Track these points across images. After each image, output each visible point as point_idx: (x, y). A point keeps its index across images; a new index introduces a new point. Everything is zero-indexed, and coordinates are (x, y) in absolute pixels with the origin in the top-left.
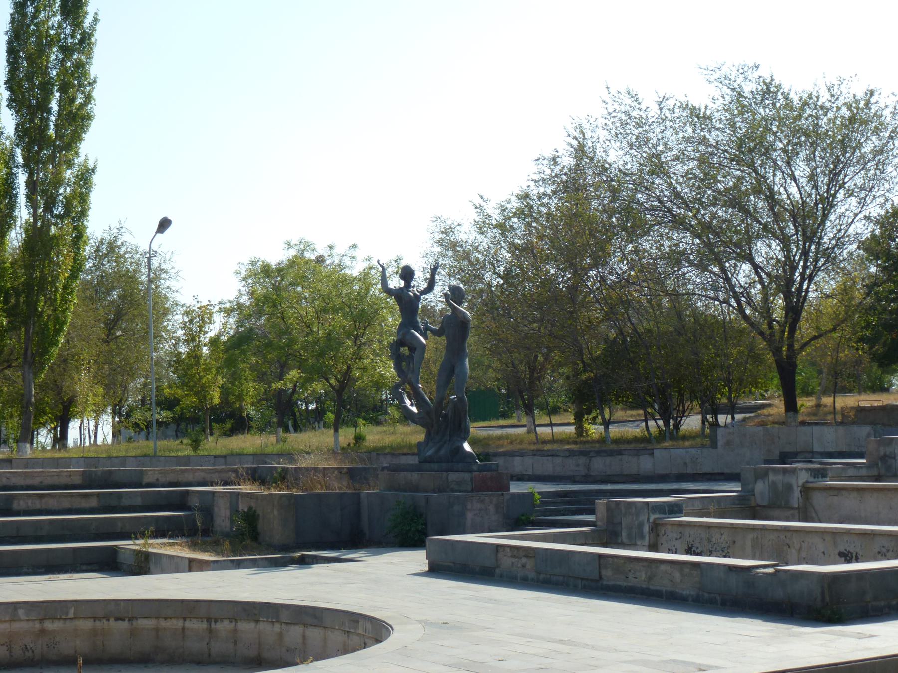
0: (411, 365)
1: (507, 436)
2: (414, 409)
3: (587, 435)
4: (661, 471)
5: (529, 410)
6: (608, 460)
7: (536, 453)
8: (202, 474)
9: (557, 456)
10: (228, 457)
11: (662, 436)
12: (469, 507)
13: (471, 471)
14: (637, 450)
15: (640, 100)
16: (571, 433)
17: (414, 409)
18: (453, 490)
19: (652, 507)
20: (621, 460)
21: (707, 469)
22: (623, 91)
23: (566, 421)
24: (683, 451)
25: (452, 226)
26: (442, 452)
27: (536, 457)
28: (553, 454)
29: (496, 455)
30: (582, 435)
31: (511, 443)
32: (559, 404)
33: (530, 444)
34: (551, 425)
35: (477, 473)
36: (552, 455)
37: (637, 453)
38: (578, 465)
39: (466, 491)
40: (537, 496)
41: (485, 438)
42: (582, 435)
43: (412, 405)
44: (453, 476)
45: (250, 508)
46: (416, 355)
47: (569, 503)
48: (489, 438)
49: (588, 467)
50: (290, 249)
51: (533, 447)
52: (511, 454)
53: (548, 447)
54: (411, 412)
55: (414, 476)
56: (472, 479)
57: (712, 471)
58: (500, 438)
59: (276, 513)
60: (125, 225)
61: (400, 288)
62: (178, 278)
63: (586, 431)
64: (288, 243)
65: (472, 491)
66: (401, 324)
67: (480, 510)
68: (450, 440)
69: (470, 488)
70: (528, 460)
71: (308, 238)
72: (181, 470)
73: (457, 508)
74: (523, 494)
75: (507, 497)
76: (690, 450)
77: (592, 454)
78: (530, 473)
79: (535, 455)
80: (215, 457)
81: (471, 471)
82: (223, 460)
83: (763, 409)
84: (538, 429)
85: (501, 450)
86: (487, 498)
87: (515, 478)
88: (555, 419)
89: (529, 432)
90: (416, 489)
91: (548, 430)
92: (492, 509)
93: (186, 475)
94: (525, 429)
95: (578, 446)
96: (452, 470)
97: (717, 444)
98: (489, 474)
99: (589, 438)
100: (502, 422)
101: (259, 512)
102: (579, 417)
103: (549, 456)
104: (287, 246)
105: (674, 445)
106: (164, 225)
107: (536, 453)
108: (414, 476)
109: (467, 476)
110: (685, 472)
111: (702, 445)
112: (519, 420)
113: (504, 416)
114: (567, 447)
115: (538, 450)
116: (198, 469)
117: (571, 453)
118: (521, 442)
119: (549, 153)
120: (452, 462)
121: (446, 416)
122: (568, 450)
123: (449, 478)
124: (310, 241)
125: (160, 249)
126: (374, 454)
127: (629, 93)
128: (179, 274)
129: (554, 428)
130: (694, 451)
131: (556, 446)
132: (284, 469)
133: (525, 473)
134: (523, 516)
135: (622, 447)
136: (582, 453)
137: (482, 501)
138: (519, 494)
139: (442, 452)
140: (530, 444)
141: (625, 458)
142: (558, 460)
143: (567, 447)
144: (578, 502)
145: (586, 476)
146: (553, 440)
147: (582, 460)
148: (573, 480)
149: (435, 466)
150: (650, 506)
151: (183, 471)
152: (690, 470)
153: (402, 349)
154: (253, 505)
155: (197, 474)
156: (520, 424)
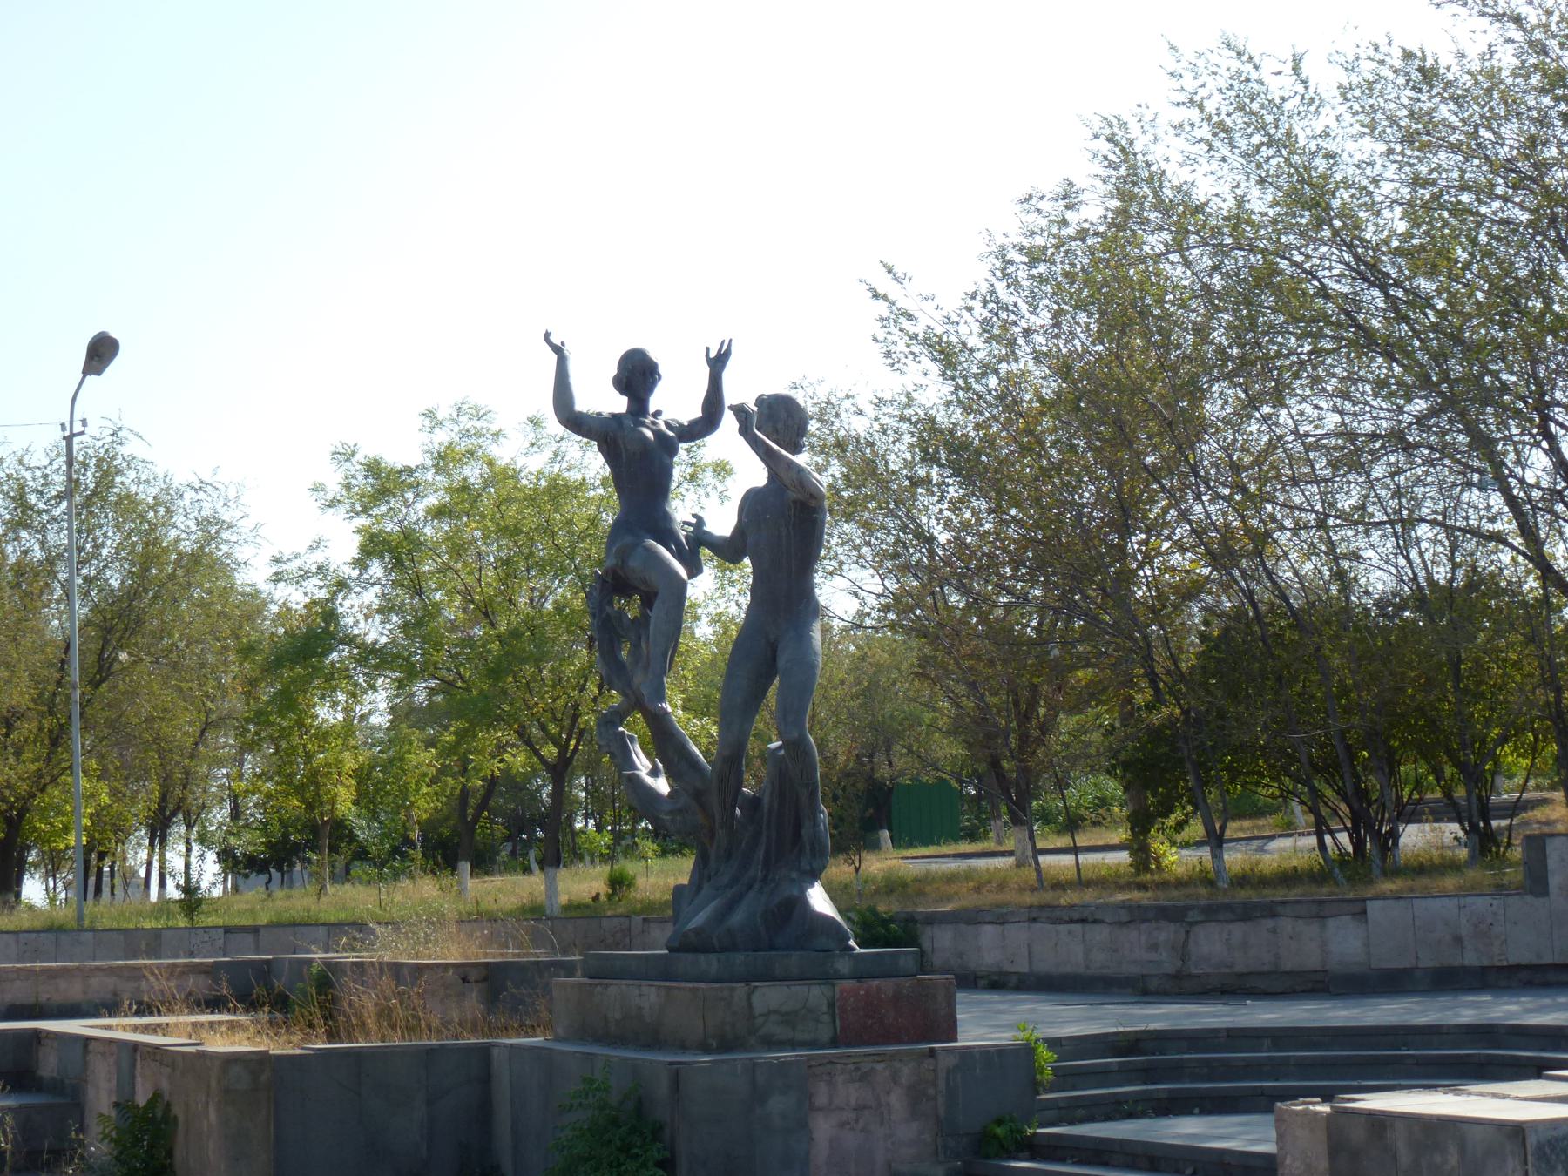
0: (643, 645)
1: (969, 875)
2: (662, 786)
3: (1159, 868)
4: (1388, 958)
5: (1020, 818)
6: (1238, 930)
7: (1039, 914)
8: (111, 982)
9: (1095, 921)
10: (262, 932)
11: (1355, 867)
12: (821, 1099)
13: (828, 978)
14: (1321, 902)
15: (1257, 60)
16: (1119, 864)
17: (662, 786)
18: (771, 1043)
19: (1540, 1147)
20: (1274, 931)
21: (1520, 954)
22: (1215, 42)
23: (1101, 843)
24: (1452, 904)
25: (833, 400)
26: (737, 918)
27: (1038, 926)
28: (1084, 918)
29: (932, 920)
30: (1147, 869)
31: (978, 889)
32: (1082, 811)
33: (1021, 890)
34: (1075, 850)
35: (849, 984)
36: (1083, 921)
37: (1320, 912)
38: (1154, 947)
39: (813, 1044)
40: (1044, 1053)
41: (916, 880)
42: (1147, 869)
43: (654, 773)
44: (769, 996)
45: (156, 1096)
46: (656, 614)
47: (1148, 1073)
48: (925, 880)
49: (1183, 953)
50: (437, 430)
51: (1029, 899)
52: (970, 918)
53: (1068, 898)
54: (652, 793)
55: (648, 996)
56: (831, 1005)
57: (1535, 961)
58: (951, 878)
59: (213, 1116)
60: (126, 423)
61: (615, 417)
62: (258, 540)
63: (1157, 860)
64: (430, 414)
65: (834, 1043)
66: (618, 526)
67: (860, 1108)
68: (765, 878)
69: (825, 1033)
70: (1018, 934)
71: (479, 399)
72: (49, 969)
73: (777, 1104)
74: (1001, 1051)
75: (945, 1062)
76: (1469, 900)
77: (1193, 916)
78: (1022, 967)
79: (1034, 920)
80: (228, 930)
81: (828, 978)
82: (250, 938)
83: (1532, 808)
84: (1041, 859)
85: (947, 908)
86: (880, 1067)
87: (982, 982)
88: (1082, 840)
89: (1019, 865)
90: (653, 1038)
91: (1068, 860)
92: (896, 1100)
93: (63, 984)
94: (1011, 860)
95: (1149, 894)
96: (768, 976)
97: (1547, 884)
98: (888, 985)
99: (1166, 876)
100: (965, 847)
101: (177, 1110)
102: (1141, 823)
103: (1071, 921)
104: (427, 422)
105: (1412, 890)
106: (101, 352)
107: (1039, 914)
108: (648, 996)
109: (816, 994)
110: (1457, 962)
111: (397, 930)
112: (1000, 843)
113: (972, 836)
114: (1120, 897)
115: (1042, 907)
116: (98, 969)
117: (1136, 915)
118: (1001, 887)
119: (1051, 185)
120: (772, 947)
121: (755, 803)
122: (1123, 905)
123: (756, 999)
124: (481, 403)
125: (217, 478)
126: (637, 920)
127: (1228, 46)
128: (261, 531)
129: (1081, 857)
130: (1481, 904)
131: (1090, 896)
132: (328, 964)
133: (1008, 968)
134: (999, 1122)
135: (1279, 894)
136: (1166, 914)
137: (865, 1078)
138: (984, 1051)
139: (737, 918)
140: (1021, 890)
141: (1286, 925)
142: (1100, 934)
143: (1120, 897)
144: (1176, 1071)
145: (1177, 977)
146: (1081, 881)
147: (1167, 933)
148: (1142, 989)
149: (710, 963)
150: (1532, 1140)
151: (52, 974)
152: (1471, 959)
153: (619, 602)
154: (165, 1085)
155: (94, 982)
156: (1002, 849)
